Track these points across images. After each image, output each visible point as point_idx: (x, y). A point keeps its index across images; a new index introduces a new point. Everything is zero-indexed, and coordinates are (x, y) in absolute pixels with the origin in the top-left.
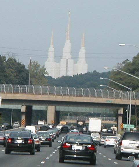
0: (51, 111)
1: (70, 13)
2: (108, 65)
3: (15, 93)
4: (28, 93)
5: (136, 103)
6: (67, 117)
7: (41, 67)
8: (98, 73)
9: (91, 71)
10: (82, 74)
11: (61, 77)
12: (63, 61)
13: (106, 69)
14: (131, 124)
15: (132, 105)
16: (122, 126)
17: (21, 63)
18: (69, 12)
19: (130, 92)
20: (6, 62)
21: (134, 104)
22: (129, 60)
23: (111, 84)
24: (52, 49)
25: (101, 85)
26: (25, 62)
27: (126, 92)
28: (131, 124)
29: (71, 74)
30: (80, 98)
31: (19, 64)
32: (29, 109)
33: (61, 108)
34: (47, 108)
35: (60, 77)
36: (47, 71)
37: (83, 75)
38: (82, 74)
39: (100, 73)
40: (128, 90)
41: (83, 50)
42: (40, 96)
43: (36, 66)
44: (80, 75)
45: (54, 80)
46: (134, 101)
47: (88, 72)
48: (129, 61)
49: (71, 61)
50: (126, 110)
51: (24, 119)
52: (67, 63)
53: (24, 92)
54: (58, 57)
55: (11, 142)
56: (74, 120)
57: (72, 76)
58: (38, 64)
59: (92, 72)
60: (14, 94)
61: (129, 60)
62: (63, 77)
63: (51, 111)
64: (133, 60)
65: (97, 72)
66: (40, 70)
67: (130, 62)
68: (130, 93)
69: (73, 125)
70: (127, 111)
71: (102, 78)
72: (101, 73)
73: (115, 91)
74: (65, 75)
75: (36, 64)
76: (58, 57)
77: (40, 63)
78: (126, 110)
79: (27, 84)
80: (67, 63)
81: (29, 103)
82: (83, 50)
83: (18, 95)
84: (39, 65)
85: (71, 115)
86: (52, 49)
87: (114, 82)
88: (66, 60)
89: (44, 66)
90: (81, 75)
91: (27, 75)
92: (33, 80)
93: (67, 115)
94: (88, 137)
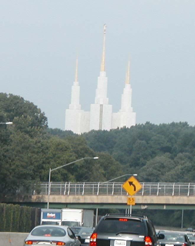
1: (106, 27)
8: (164, 125)
11: (91, 131)
12: (95, 108)
17: (89, 131)
18: (105, 26)
24: (76, 89)
29: (107, 127)
38: (125, 127)
39: (77, 135)
41: (128, 90)
44: (121, 128)
47: (136, 125)
49: (108, 108)
52: (101, 111)
54: (86, 103)
55: (94, 132)
57: (176, 123)
59: (143, 124)
69: (99, 165)
72: (167, 123)
74: (97, 129)
76: (86, 103)
80: (101, 111)
82: (128, 90)
86: (76, 89)
88: (99, 105)
90: (125, 129)
94: (135, 232)
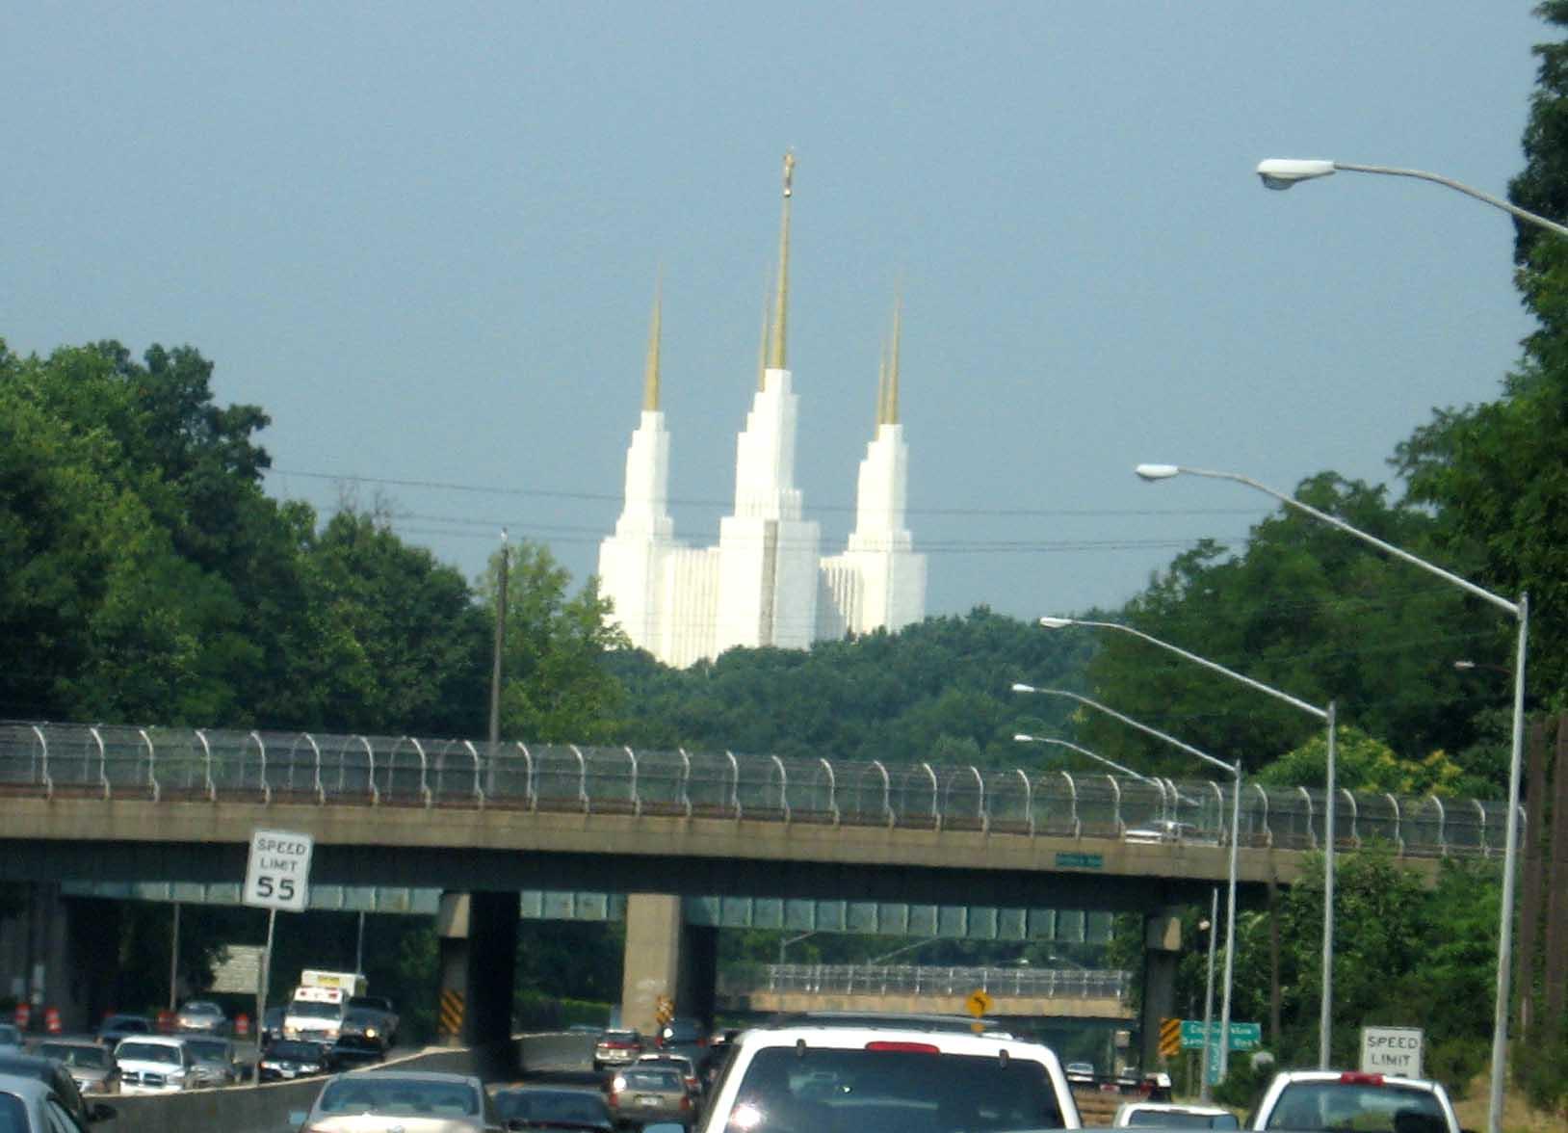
0: (650, 926)
2: (1080, 572)
3: (390, 804)
4: (490, 803)
5: (1273, 870)
6: (773, 969)
7: (571, 593)
9: (958, 608)
10: (889, 631)
11: (720, 658)
12: (742, 533)
13: (1148, 478)
14: (1237, 1016)
15: (1238, 884)
16: (1177, 1038)
19: (1232, 788)
20: (314, 548)
21: (1257, 874)
22: (1221, 550)
23: (1097, 731)
25: (1019, 737)
26: (465, 554)
27: (1203, 790)
28: (1237, 1016)
30: (865, 833)
31: (416, 566)
32: (497, 915)
33: (731, 912)
34: (624, 910)
35: (714, 659)
36: (616, 625)
37: (893, 637)
40: (1223, 777)
41: (880, 470)
42: (578, 821)
43: (546, 581)
45: (674, 680)
46: (1262, 854)
47: (928, 619)
48: (1221, 560)
50: (1204, 925)
51: (462, 994)
53: (457, 787)
56: (955, 993)
58: (552, 570)
60: (385, 809)
61: (1221, 550)
62: (736, 657)
63: (650, 926)
64: (1252, 544)
65: (997, 618)
66: (571, 614)
67: (1233, 562)
68: (1228, 797)
70: (1207, 931)
71: (1031, 689)
73: (1123, 778)
74: (752, 641)
75: (542, 568)
77: (561, 558)
78: (1204, 925)
79: (479, 733)
81: (493, 876)
83: (417, 816)
84: (561, 575)
85: (798, 955)
87: (1108, 711)
89: (593, 583)
91: (482, 659)
92: (520, 691)
93: (773, 958)
